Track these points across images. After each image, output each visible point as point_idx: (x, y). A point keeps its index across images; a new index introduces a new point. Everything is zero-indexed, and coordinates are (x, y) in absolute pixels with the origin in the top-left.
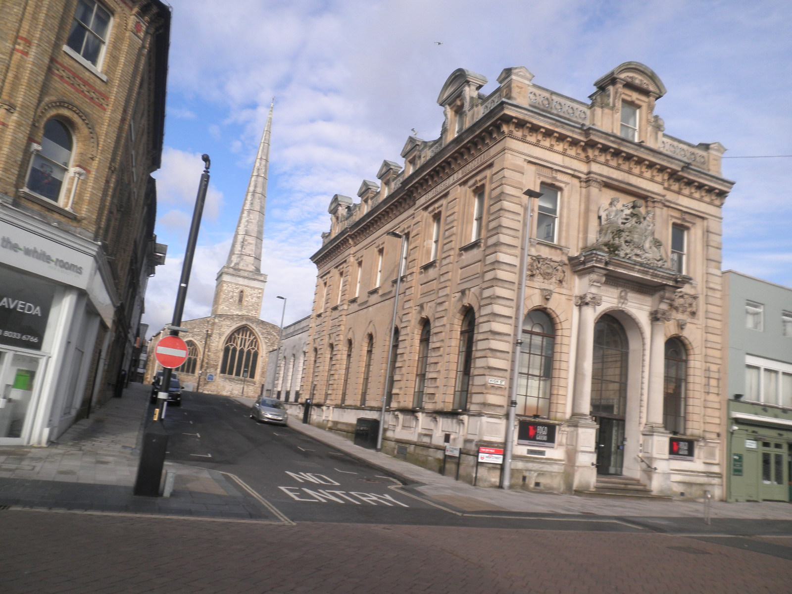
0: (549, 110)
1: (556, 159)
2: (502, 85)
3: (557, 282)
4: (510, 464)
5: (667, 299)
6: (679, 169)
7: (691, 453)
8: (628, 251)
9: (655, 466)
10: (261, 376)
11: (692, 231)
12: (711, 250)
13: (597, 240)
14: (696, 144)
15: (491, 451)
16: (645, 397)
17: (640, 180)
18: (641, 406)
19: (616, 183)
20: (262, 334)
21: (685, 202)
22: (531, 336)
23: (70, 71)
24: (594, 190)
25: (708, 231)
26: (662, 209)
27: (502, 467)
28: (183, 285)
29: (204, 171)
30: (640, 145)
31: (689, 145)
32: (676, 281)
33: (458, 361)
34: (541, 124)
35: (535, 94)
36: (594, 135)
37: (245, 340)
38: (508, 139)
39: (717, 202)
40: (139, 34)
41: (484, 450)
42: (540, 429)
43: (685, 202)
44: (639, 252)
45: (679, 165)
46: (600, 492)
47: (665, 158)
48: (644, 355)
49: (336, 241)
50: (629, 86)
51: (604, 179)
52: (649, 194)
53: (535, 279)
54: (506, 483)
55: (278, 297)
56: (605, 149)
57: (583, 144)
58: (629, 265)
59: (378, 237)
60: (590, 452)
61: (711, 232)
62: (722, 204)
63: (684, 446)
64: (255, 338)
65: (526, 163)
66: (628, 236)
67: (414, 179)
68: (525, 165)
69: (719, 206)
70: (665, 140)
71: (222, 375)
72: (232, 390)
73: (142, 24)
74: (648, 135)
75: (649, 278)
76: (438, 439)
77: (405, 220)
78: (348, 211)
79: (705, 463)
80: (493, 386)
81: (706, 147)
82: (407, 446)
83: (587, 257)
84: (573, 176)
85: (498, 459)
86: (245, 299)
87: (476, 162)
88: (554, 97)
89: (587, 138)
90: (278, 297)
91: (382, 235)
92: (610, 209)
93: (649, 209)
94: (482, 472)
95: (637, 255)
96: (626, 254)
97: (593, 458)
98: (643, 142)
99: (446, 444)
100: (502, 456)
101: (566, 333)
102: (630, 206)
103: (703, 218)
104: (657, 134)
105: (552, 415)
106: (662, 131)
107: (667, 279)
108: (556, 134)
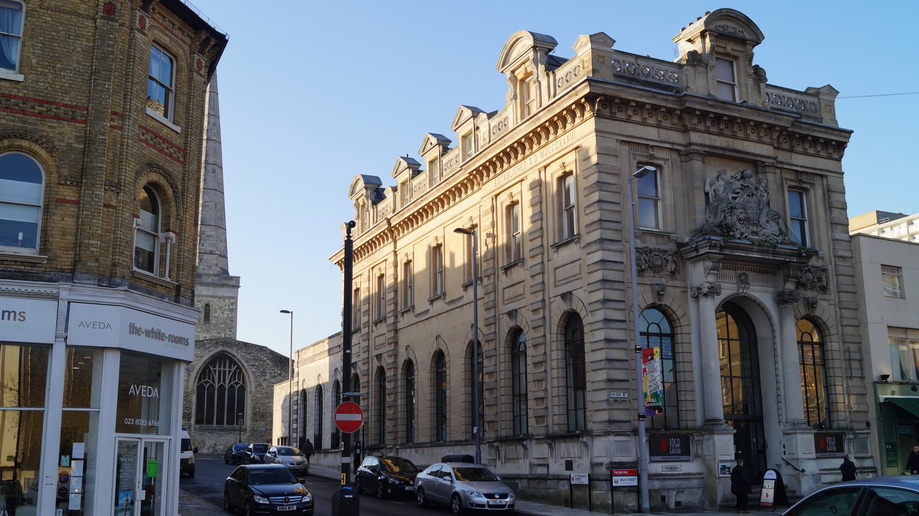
0: (636, 77)
1: (651, 133)
3: (669, 273)
4: (646, 485)
5: (792, 277)
6: (789, 125)
9: (802, 468)
10: (253, 420)
11: (812, 192)
12: (836, 212)
15: (625, 472)
17: (746, 143)
19: (721, 152)
20: (247, 362)
21: (801, 161)
22: (648, 339)
23: (152, 133)
24: (697, 164)
25: (829, 191)
28: (348, 351)
30: (744, 104)
31: (797, 92)
33: (567, 375)
34: (631, 98)
35: (618, 61)
36: (691, 101)
37: (225, 372)
39: (836, 156)
40: (200, 72)
41: (617, 473)
42: (672, 441)
43: (801, 161)
44: (755, 229)
48: (774, 344)
51: (707, 149)
52: (759, 159)
53: (645, 274)
54: (646, 505)
55: (283, 311)
56: (704, 115)
57: (678, 112)
61: (833, 192)
64: (238, 368)
65: (618, 144)
66: (741, 213)
70: (769, 91)
71: (197, 426)
72: (215, 445)
73: (202, 60)
74: (750, 90)
76: (557, 468)
78: (377, 194)
80: (616, 401)
82: (517, 481)
83: (699, 244)
85: (631, 481)
86: (213, 315)
88: (639, 61)
89: (682, 105)
90: (283, 311)
93: (760, 176)
96: (742, 234)
98: (745, 102)
99: (568, 473)
100: (636, 477)
101: (685, 329)
102: (739, 177)
103: (822, 176)
104: (759, 86)
107: (790, 255)
108: (647, 107)
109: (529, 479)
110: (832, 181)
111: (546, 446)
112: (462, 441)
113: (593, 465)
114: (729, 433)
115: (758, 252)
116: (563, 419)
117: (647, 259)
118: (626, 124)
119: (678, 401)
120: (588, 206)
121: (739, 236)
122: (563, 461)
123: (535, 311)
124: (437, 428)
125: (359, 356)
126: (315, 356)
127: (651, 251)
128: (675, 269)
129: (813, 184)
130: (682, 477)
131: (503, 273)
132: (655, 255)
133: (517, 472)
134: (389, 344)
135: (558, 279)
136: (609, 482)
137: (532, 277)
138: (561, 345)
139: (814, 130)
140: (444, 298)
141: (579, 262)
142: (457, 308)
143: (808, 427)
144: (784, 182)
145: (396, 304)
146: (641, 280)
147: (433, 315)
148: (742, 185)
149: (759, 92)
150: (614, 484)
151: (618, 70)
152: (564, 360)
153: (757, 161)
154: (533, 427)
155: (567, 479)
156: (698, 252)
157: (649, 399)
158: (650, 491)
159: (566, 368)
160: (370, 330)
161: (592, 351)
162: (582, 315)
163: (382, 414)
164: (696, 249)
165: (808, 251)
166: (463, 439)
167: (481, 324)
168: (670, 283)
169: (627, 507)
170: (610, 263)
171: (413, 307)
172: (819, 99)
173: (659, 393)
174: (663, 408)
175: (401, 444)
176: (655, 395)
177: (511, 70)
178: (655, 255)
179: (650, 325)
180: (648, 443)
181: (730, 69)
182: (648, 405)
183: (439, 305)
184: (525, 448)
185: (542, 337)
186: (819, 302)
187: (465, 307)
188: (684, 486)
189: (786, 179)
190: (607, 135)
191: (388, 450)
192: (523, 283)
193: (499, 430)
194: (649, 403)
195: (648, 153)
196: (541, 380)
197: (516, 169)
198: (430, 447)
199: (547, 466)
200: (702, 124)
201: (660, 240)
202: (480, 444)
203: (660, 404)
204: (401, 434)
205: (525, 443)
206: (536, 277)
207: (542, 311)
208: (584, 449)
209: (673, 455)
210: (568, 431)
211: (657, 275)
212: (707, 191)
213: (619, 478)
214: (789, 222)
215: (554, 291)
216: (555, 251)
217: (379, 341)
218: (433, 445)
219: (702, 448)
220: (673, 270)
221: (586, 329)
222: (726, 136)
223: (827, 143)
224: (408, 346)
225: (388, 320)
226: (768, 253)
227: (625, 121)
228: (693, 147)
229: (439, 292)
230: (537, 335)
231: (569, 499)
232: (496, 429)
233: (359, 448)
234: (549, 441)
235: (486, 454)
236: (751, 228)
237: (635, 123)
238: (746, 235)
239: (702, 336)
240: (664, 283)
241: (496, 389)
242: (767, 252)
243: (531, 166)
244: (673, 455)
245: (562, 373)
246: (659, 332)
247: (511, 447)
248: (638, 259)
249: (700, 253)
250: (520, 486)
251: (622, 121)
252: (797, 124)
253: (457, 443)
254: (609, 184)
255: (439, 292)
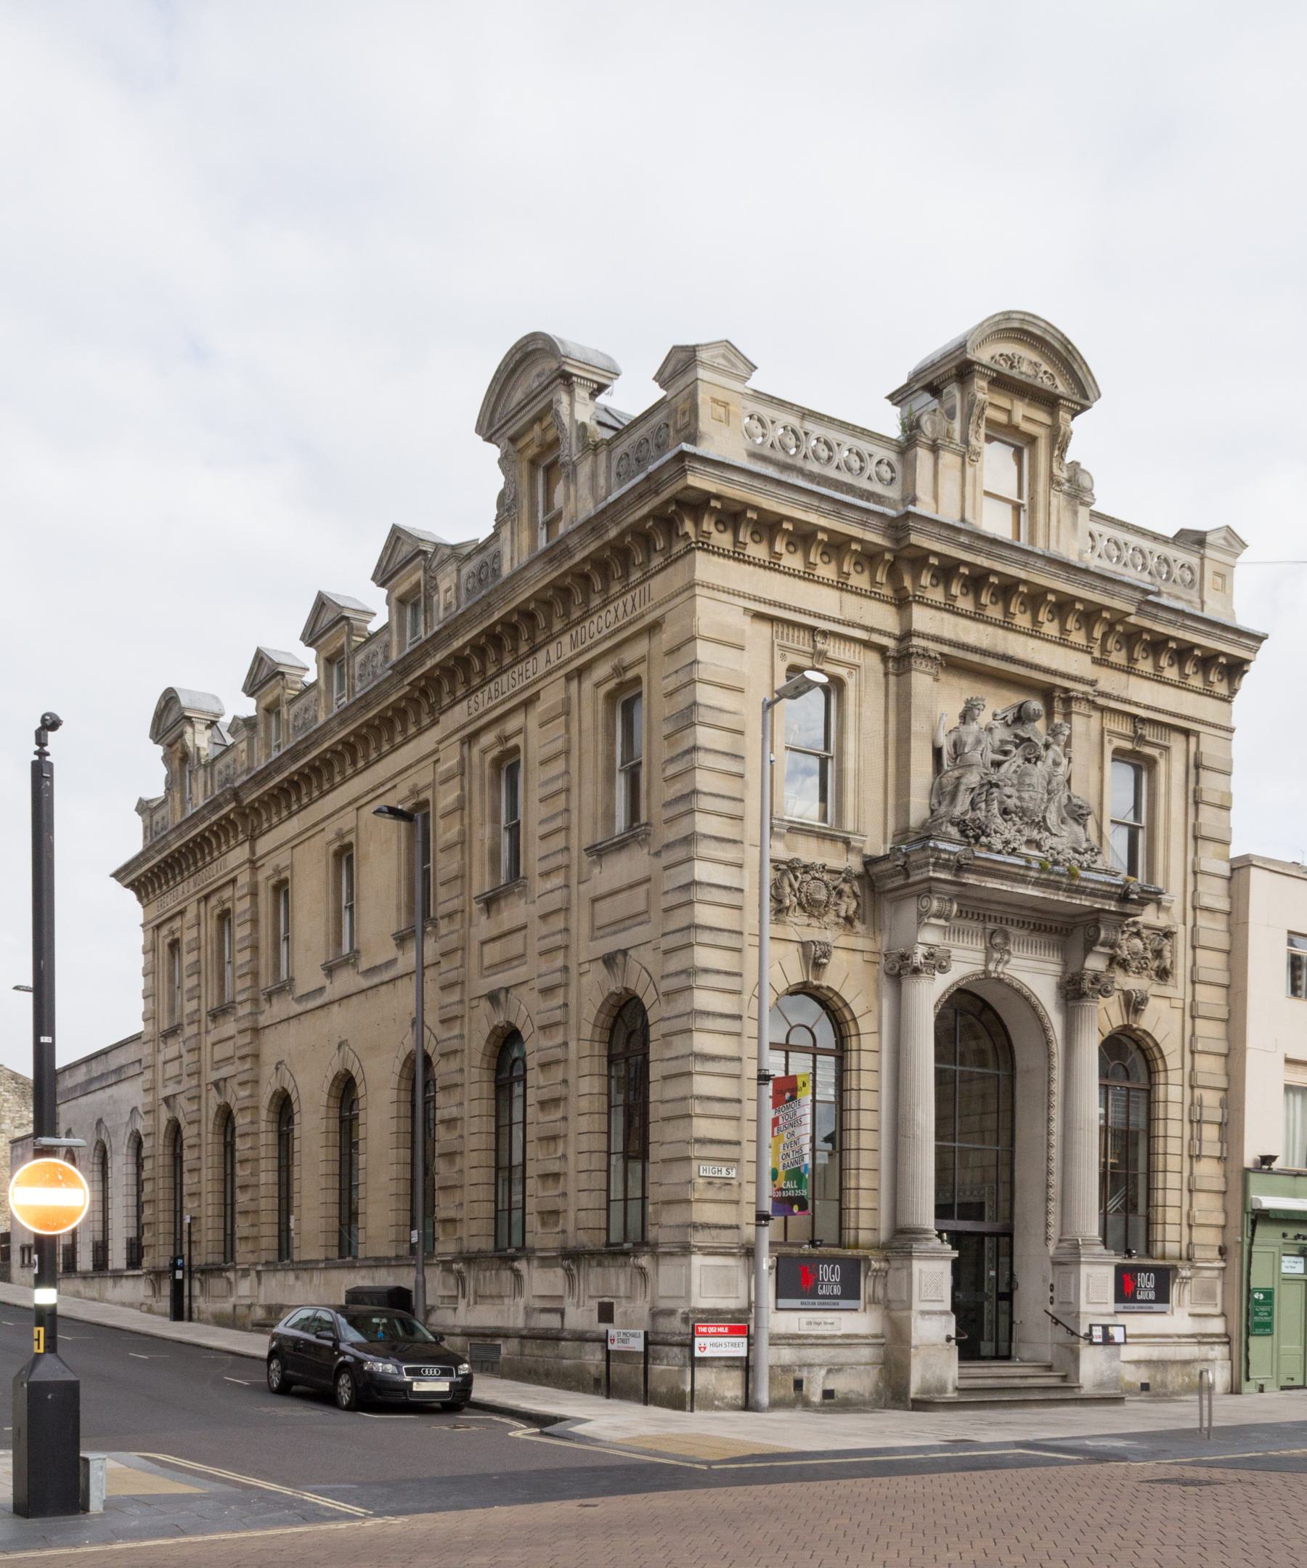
2: (673, 392)
3: (841, 920)
4: (768, 1356)
5: (1103, 945)
6: (1132, 609)
7: (1162, 1296)
8: (1007, 836)
12: (1207, 814)
13: (932, 811)
14: (1171, 533)
15: (721, 1330)
16: (1055, 1179)
18: (1048, 1199)
19: (976, 658)
26: (1089, 716)
27: (746, 1367)
28: (45, 1039)
29: (36, 753)
31: (1156, 537)
32: (1124, 898)
36: (920, 531)
38: (699, 555)
42: (824, 1271)
44: (1035, 834)
45: (1130, 600)
46: (970, 1399)
47: (1097, 583)
49: (196, 826)
50: (1002, 383)
53: (788, 919)
54: (764, 1397)
55: (17, 988)
56: (947, 571)
58: (1016, 870)
59: (332, 815)
60: (943, 1313)
62: (1233, 692)
63: (1146, 1282)
65: (748, 619)
67: (428, 655)
68: (747, 624)
69: (1227, 700)
70: (1096, 527)
75: (1062, 898)
76: (580, 1316)
77: (410, 767)
79: (1191, 1315)
81: (1194, 540)
82: (499, 1342)
84: (867, 644)
85: (736, 1347)
87: (611, 617)
88: (809, 426)
90: (17, 988)
91: (343, 808)
92: (963, 728)
94: (704, 1378)
95: (1029, 842)
96: (1007, 843)
97: (949, 1325)
100: (745, 1340)
103: (1186, 733)
104: (1075, 513)
105: (850, 1236)
106: (1088, 504)
109: (523, 1337)
110: (1209, 745)
111: (560, 1272)
112: (389, 1259)
113: (656, 1314)
114: (943, 1258)
115: (1037, 883)
116: (598, 1219)
117: (796, 885)
118: (767, 573)
119: (841, 1190)
120: (672, 760)
121: (1000, 847)
122: (594, 1304)
123: (547, 991)
124: (340, 1232)
125: (179, 1082)
126: (91, 1081)
127: (807, 869)
128: (855, 912)
129: (1167, 749)
130: (839, 1341)
131: (481, 910)
132: (814, 878)
133: (499, 1323)
134: (242, 1058)
135: (598, 923)
136: (687, 1350)
137: (544, 917)
138: (600, 1065)
139: (1184, 627)
140: (355, 965)
141: (645, 887)
142: (382, 984)
143: (1105, 1252)
144: (1106, 738)
145: (255, 975)
146: (779, 931)
147: (332, 998)
148: (1016, 736)
149: (1075, 525)
150: (698, 1354)
151: (759, 440)
152: (605, 1098)
153: (1054, 687)
154: (539, 1236)
155: (600, 1340)
156: (908, 876)
157: (781, 1182)
158: (771, 1367)
159: (609, 1114)
160: (203, 1029)
161: (665, 1078)
162: (647, 1002)
163: (229, 1201)
164: (905, 870)
165: (1143, 891)
166: (392, 1254)
167: (431, 1019)
168: (844, 941)
169: (723, 1398)
170: (714, 890)
171: (291, 980)
172: (1202, 558)
173: (802, 1170)
174: (810, 1203)
175: (267, 1263)
176: (795, 1175)
177: (511, 432)
178: (814, 878)
179: (792, 1028)
180: (774, 1271)
181: (1015, 468)
182: (779, 1194)
183: (347, 981)
184: (517, 1275)
185: (559, 1046)
186: (1152, 1001)
187: (399, 983)
188: (842, 1360)
189: (1111, 732)
190: (724, 597)
191: (240, 1273)
192: (523, 932)
193: (465, 1236)
194: (781, 1190)
195: (815, 647)
196: (554, 1138)
197: (516, 676)
198: (326, 1268)
199: (562, 1313)
200: (940, 589)
201: (827, 845)
202: (424, 1265)
203: (805, 1193)
204: (269, 1239)
205: (516, 1264)
206: (552, 919)
207: (561, 991)
208: (638, 1280)
209: (824, 1297)
210: (608, 1244)
211: (814, 922)
212: (939, 745)
213: (707, 1341)
214: (1107, 828)
215: (587, 949)
216: (593, 863)
217: (220, 1052)
218: (329, 1265)
219: (886, 1285)
220: (851, 912)
221: (654, 1033)
222: (991, 624)
223: (1207, 661)
224: (280, 1063)
225: (239, 1007)
226: (1059, 889)
227: (765, 567)
228: (915, 641)
229: (346, 949)
230: (550, 1044)
231: (603, 1382)
232: (458, 1235)
233: (181, 1268)
234: (566, 1263)
235: (436, 1286)
236: (1026, 831)
237: (790, 575)
238: (1015, 845)
239: (902, 1055)
240: (829, 940)
241: (462, 1153)
242: (1056, 886)
243: (550, 667)
244: (824, 1297)
245: (599, 1123)
246: (810, 1044)
247: (488, 1274)
248: (777, 885)
249: (911, 880)
250: (503, 1351)
251: (760, 566)
252: (1149, 609)
253: (379, 1263)
254: (721, 710)
255: (346, 949)
